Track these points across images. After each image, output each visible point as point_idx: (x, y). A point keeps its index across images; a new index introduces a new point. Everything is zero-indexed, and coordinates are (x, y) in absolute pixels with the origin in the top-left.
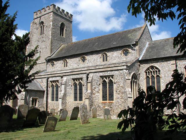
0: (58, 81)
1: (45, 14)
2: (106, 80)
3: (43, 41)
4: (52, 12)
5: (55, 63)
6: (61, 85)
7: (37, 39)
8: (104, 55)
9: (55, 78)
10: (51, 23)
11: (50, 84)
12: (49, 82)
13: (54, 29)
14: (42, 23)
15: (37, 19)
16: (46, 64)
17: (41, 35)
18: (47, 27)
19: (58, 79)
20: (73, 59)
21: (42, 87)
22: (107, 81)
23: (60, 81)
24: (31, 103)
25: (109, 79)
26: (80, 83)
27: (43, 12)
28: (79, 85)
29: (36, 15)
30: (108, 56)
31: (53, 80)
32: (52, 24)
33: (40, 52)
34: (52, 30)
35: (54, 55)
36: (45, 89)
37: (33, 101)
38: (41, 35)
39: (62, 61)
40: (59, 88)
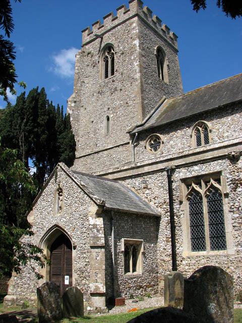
0: (217, 176)
1: (113, 25)
2: (197, 188)
3: (116, 89)
4: (136, 15)
5: (163, 138)
6: (235, 189)
7: (96, 88)
8: (199, 130)
9: (204, 166)
10: (137, 42)
11: (182, 191)
12: (174, 185)
13: (143, 56)
14: (109, 47)
15: (93, 43)
16: (131, 146)
17: (106, 76)
18: (122, 54)
19: (218, 169)
20: (230, 118)
21: (146, 205)
22: (202, 191)
23: (226, 176)
24: (122, 257)
25: (207, 185)
26: (210, 192)
27: (108, 23)
28: (207, 196)
29: (88, 35)
30: (211, 131)
31: (194, 174)
32: (141, 44)
33: (108, 119)
34: (140, 59)
35: (155, 117)
36: (162, 211)
37: (126, 253)
38: (106, 76)
39: (189, 131)
40: (225, 201)
